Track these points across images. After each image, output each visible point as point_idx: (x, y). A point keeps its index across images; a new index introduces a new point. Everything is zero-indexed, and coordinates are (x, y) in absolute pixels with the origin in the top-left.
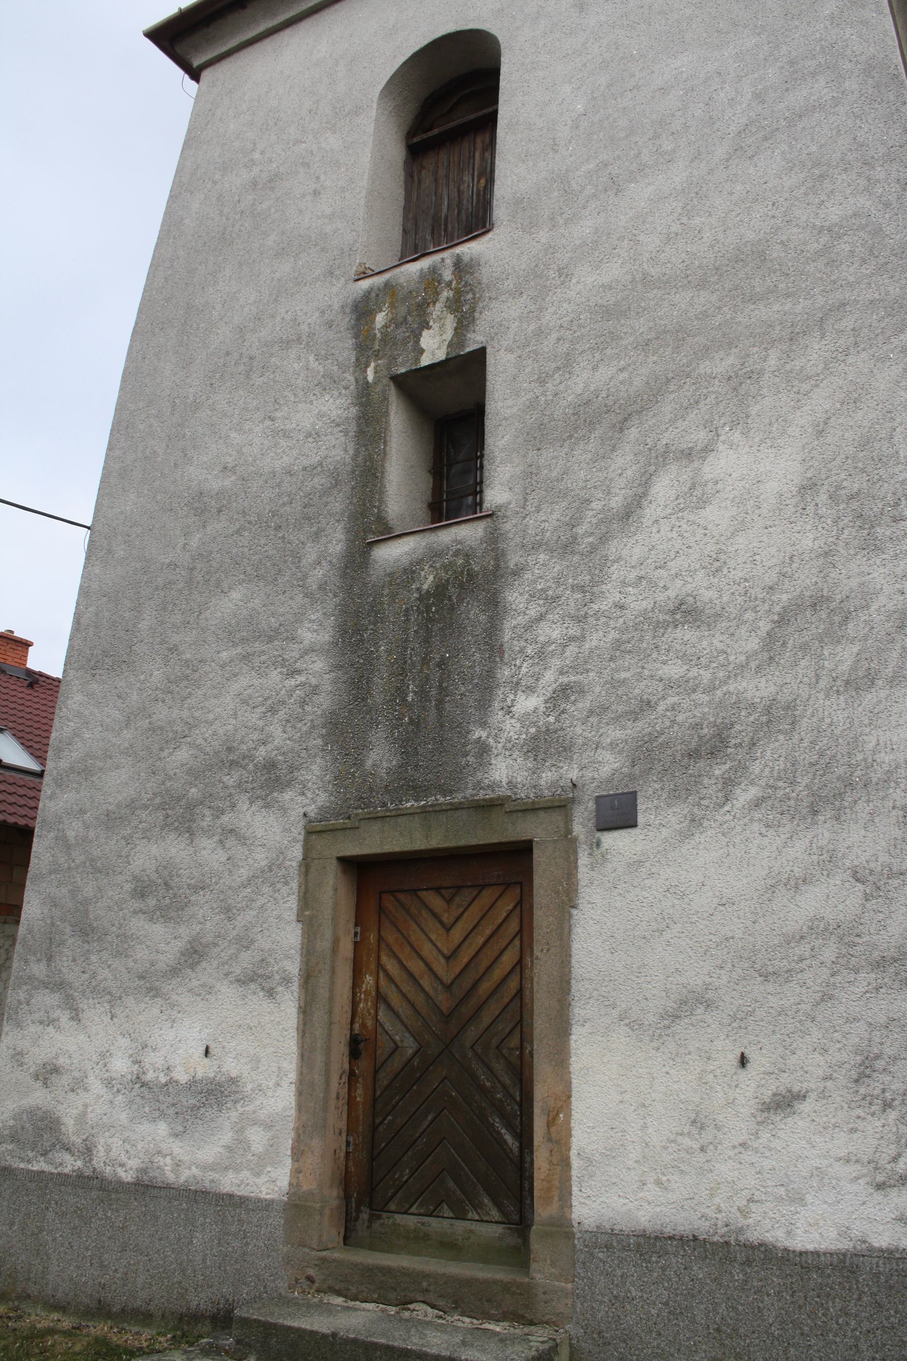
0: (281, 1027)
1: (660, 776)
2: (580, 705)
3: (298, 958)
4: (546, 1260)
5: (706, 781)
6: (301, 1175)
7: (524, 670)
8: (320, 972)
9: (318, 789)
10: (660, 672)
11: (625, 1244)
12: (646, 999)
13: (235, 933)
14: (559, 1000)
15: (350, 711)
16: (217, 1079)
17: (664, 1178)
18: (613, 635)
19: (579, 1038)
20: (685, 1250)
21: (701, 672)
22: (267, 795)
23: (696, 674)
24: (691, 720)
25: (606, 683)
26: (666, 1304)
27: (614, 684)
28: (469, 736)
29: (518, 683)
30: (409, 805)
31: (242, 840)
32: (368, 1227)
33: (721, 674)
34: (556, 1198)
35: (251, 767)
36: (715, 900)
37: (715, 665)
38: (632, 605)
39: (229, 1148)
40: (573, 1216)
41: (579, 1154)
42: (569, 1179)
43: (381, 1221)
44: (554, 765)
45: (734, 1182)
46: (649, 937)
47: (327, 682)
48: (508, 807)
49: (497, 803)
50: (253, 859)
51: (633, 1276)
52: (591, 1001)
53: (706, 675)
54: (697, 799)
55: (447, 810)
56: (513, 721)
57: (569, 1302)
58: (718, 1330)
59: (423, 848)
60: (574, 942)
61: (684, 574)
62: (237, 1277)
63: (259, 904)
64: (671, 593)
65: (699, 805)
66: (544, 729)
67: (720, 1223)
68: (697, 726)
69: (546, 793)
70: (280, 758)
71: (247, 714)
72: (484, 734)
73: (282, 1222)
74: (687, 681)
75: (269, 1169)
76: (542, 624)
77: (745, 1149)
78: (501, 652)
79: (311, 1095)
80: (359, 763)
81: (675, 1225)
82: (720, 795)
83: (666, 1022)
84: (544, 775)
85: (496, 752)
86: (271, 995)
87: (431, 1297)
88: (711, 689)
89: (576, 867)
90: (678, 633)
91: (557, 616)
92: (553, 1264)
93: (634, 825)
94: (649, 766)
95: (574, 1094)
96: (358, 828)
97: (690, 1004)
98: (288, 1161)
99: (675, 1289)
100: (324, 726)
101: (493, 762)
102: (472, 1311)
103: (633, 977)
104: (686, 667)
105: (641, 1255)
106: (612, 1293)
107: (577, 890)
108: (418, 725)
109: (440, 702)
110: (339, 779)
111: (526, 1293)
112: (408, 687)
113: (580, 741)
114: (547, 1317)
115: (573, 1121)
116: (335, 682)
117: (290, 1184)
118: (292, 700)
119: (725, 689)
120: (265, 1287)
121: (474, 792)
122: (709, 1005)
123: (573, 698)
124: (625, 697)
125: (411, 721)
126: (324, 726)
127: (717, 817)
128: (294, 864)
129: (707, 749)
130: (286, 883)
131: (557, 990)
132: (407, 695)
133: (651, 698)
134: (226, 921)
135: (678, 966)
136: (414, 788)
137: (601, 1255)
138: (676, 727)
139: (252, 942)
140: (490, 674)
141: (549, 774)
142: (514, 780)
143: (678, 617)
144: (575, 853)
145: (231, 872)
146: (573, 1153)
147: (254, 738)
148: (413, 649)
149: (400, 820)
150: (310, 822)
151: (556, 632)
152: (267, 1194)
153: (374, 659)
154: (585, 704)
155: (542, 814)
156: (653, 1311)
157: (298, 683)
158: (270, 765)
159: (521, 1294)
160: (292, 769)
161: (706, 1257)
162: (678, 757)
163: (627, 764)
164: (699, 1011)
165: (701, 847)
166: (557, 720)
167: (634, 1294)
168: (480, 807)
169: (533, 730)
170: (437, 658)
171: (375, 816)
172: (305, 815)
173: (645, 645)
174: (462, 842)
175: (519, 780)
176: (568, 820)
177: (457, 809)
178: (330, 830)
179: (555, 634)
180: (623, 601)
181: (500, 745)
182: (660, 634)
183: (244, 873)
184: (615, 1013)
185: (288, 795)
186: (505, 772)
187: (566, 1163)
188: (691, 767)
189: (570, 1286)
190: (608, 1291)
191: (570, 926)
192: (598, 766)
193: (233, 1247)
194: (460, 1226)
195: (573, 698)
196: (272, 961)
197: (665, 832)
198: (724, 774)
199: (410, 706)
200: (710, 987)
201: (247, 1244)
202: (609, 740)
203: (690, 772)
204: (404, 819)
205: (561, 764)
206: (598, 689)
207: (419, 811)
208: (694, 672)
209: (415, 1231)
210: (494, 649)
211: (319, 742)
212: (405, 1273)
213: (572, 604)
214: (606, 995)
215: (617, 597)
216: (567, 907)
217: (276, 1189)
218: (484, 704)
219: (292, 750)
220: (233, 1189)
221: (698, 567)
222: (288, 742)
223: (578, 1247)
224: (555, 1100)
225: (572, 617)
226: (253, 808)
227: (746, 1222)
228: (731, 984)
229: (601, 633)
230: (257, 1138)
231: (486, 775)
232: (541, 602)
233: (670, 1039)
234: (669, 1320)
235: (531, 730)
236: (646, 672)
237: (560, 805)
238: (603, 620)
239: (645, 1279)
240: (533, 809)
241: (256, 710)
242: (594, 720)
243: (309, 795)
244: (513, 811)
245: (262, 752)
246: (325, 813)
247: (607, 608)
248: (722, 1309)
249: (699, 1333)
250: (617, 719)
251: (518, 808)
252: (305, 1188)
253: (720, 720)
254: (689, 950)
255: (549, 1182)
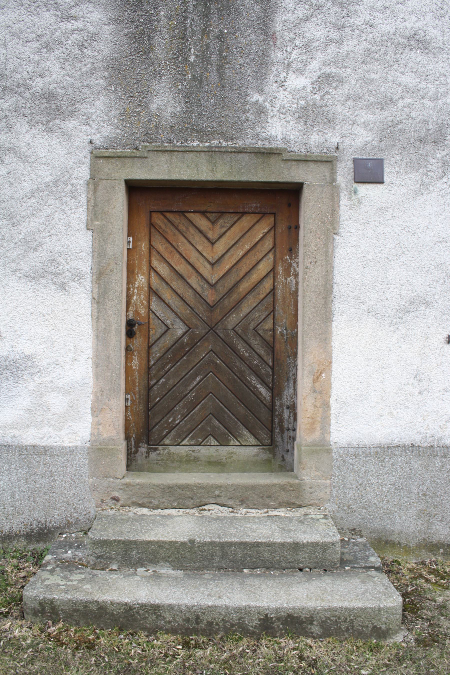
0: (75, 314)
1: (400, 151)
2: (340, 91)
3: (89, 259)
4: (312, 468)
5: (431, 160)
6: (100, 427)
7: (294, 56)
8: (112, 270)
9: (104, 121)
10: (400, 79)
11: (367, 453)
12: (387, 299)
13: (21, 237)
14: (323, 298)
15: (132, 61)
16: (11, 357)
17: (395, 412)
18: (364, 45)
19: (339, 325)
20: (406, 453)
21: (429, 85)
22: (48, 122)
23: (425, 87)
24: (421, 117)
25: (360, 79)
26: (394, 484)
27: (366, 81)
28: (248, 98)
29: (289, 65)
30: (195, 144)
31: (24, 158)
32: (146, 457)
33: (442, 90)
34: (318, 429)
35: (28, 95)
36: (435, 238)
37: (437, 83)
38: (379, 26)
39: (29, 411)
40: (331, 439)
41: (337, 400)
42: (329, 416)
43: (158, 452)
44: (320, 131)
45: (438, 411)
46: (390, 259)
47: (106, 31)
48: (285, 156)
49: (275, 152)
50: (36, 175)
51: (372, 471)
52: (348, 299)
53: (432, 89)
54: (425, 171)
55: (231, 152)
56: (286, 93)
57: (328, 491)
58: (425, 495)
59: (209, 179)
60: (336, 258)
61: (417, 12)
62: (47, 504)
63: (45, 213)
64: (409, 24)
65: (427, 175)
66: (311, 103)
67: (428, 435)
68: (425, 122)
69: (314, 150)
70: (60, 91)
71: (19, 47)
72: (261, 99)
73: (87, 462)
74: (419, 90)
75: (70, 424)
76: (308, 24)
77: (447, 392)
78: (275, 40)
79: (107, 367)
80: (143, 104)
81: (401, 439)
82: (440, 171)
83: (400, 314)
84: (312, 137)
85: (272, 114)
86: (64, 289)
87: (222, 500)
88: (434, 99)
89: (339, 206)
90: (413, 55)
91: (320, 21)
92: (317, 470)
93: (383, 183)
94: (393, 143)
95: (334, 360)
96: (146, 157)
97: (415, 304)
98: (89, 418)
99: (400, 476)
100: (106, 69)
101: (269, 120)
102: (255, 505)
103: (378, 285)
104: (418, 80)
105: (378, 458)
106: (358, 482)
107: (339, 222)
108: (201, 82)
109: (220, 69)
110: (124, 116)
111: (297, 489)
112: (189, 50)
113: (340, 117)
114: (312, 502)
115: (333, 379)
116: (114, 33)
117: (92, 434)
118: (70, 42)
119: (444, 101)
120: (75, 509)
121: (253, 141)
122: (428, 305)
123: (334, 85)
124: (374, 92)
125: (194, 78)
126: (106, 69)
127: (438, 185)
128: (81, 182)
129: (432, 138)
130: (74, 198)
131: (322, 291)
132: (189, 56)
133: (393, 96)
134: (10, 227)
135: (409, 279)
136: (198, 132)
137: (351, 461)
138: (410, 120)
139: (40, 245)
140: (265, 53)
141: (317, 137)
142: (288, 137)
143: (413, 43)
144: (338, 195)
145: (11, 184)
146: (332, 400)
147: (29, 70)
148: (193, 20)
149: (187, 155)
150: (96, 148)
151: (320, 33)
152: (70, 443)
153: (154, 21)
154: (344, 91)
155: (312, 165)
156: (385, 490)
157: (74, 27)
158: (49, 96)
159: (293, 490)
160: (73, 101)
161: (420, 455)
162: (412, 141)
163: (376, 139)
164: (422, 308)
165: (427, 203)
166: (322, 98)
167: (373, 481)
168: (260, 153)
169: (302, 103)
170: (217, 32)
171: (164, 149)
172: (91, 142)
173: (388, 57)
174: (244, 178)
175: (292, 137)
176: (333, 172)
177: (240, 152)
178: (119, 157)
179: (319, 34)
180: (372, 21)
181: (275, 110)
182: (400, 53)
183: (27, 186)
184: (365, 308)
185: (70, 124)
186: (281, 130)
187: (327, 406)
188: (421, 149)
189: (328, 481)
190: (355, 482)
191: (334, 247)
192: (355, 137)
193: (41, 484)
194: (224, 450)
195: (334, 85)
196: (63, 261)
197: (403, 190)
198: (443, 157)
199: (192, 65)
200: (429, 294)
201: (54, 480)
202: (362, 120)
203: (420, 152)
204: (191, 155)
205: (326, 131)
206: (353, 82)
207: (206, 150)
208: (423, 85)
209: (187, 456)
210: (268, 35)
211: (102, 82)
212: (200, 487)
213: (333, 14)
214: (359, 295)
215: (368, 18)
216: (332, 233)
217: (78, 438)
218: (261, 76)
219: (73, 86)
220: (35, 441)
221: (428, 10)
222: (68, 78)
223: (335, 458)
224: (319, 365)
225: (333, 25)
226: (33, 131)
227: (444, 434)
228: (443, 292)
229: (356, 42)
230: (57, 402)
231: (263, 130)
232: (307, 7)
233: (403, 325)
234: (395, 493)
235: (301, 102)
236: (389, 77)
237: (328, 161)
238: (357, 32)
239: (381, 472)
240: (305, 160)
241: (28, 44)
242: (350, 103)
243: (94, 125)
244: (289, 160)
245: (38, 84)
246: (110, 143)
247: (360, 24)
248: (428, 483)
249: (413, 498)
250: (368, 106)
251: (294, 158)
252: (105, 435)
253: (440, 121)
254: (417, 269)
255: (313, 418)
